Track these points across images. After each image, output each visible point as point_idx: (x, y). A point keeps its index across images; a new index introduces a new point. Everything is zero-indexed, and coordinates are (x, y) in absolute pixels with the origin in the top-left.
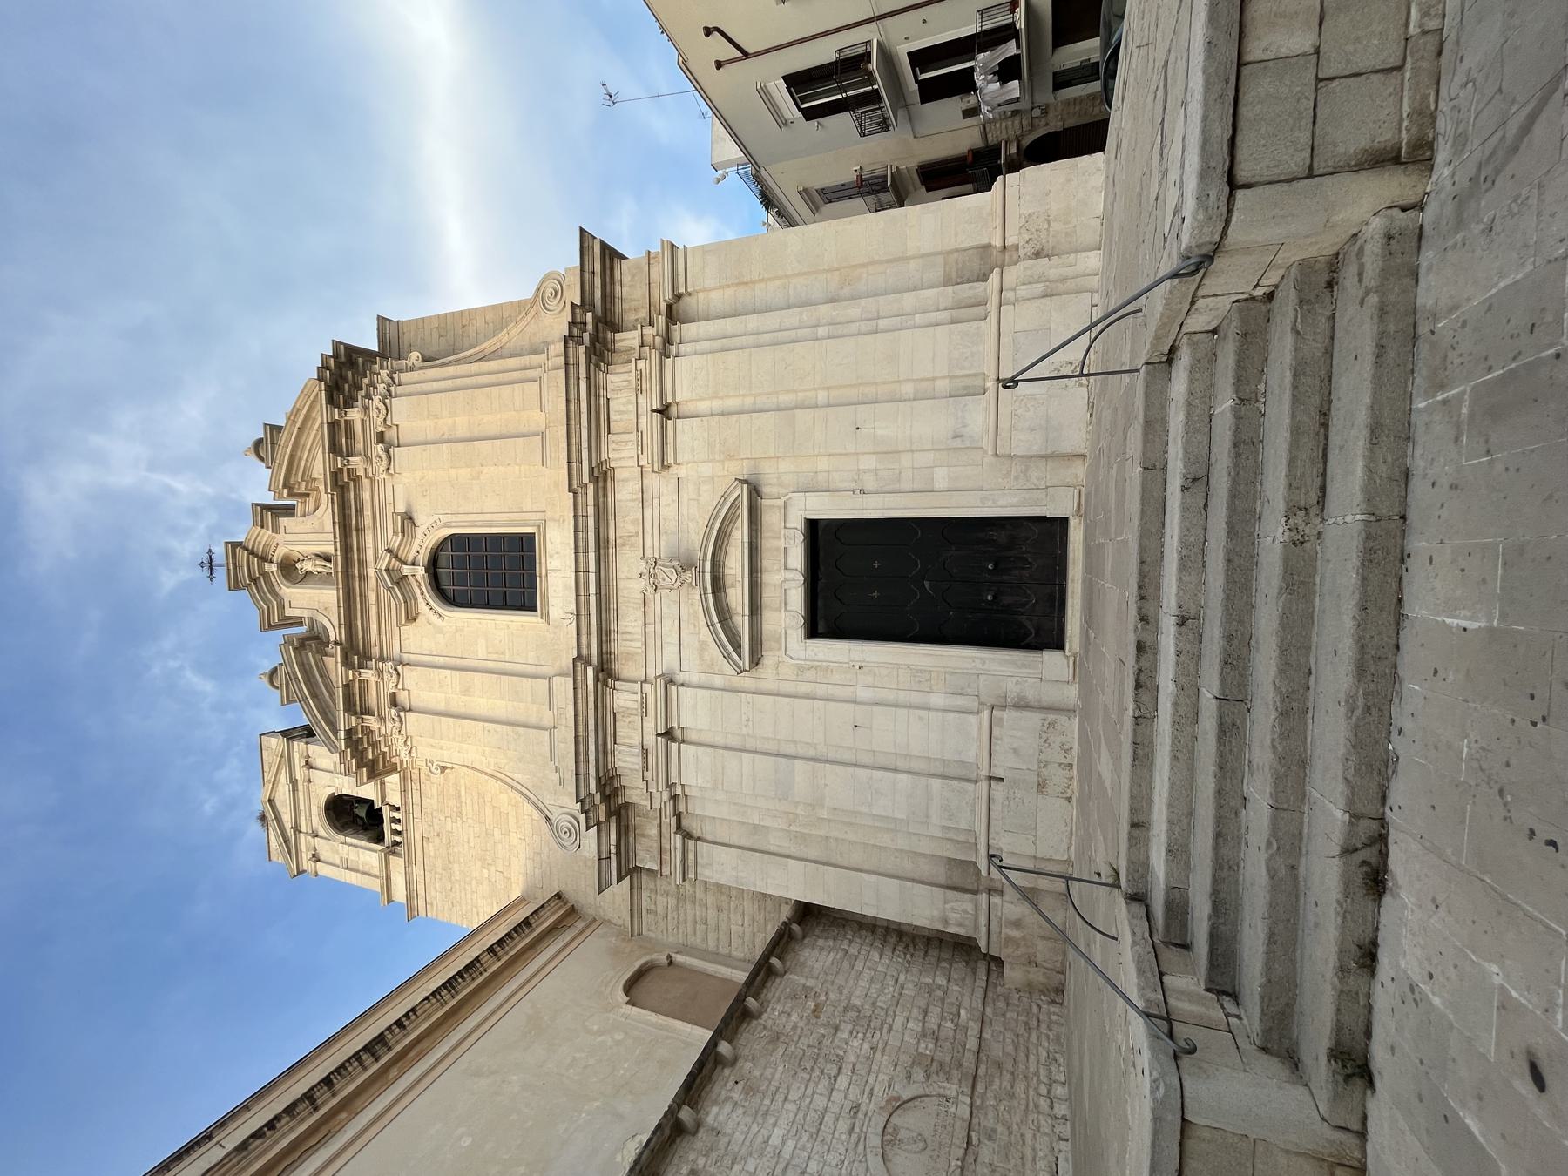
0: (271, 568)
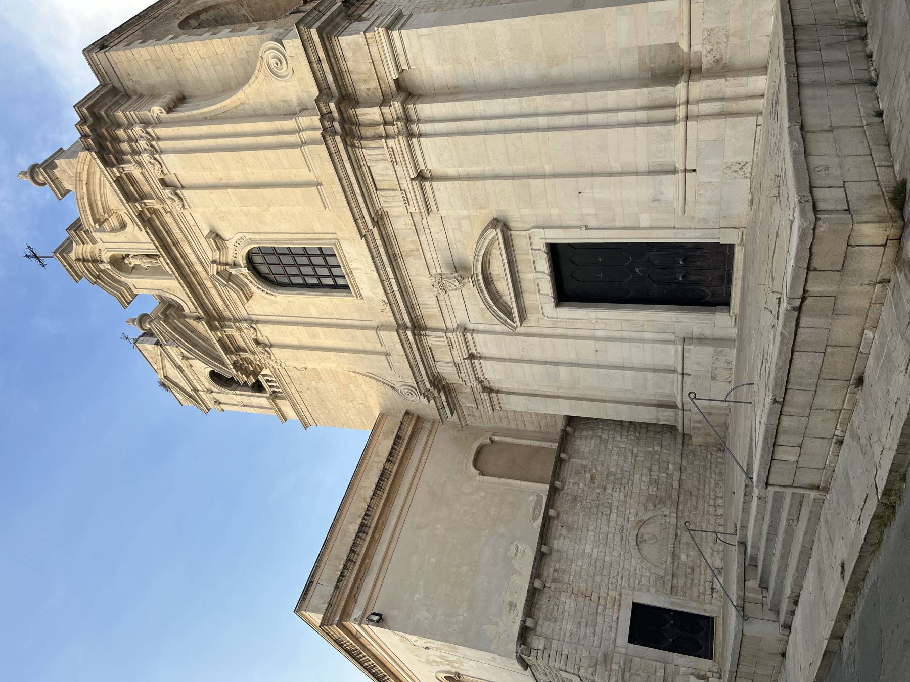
0: (106, 266)
